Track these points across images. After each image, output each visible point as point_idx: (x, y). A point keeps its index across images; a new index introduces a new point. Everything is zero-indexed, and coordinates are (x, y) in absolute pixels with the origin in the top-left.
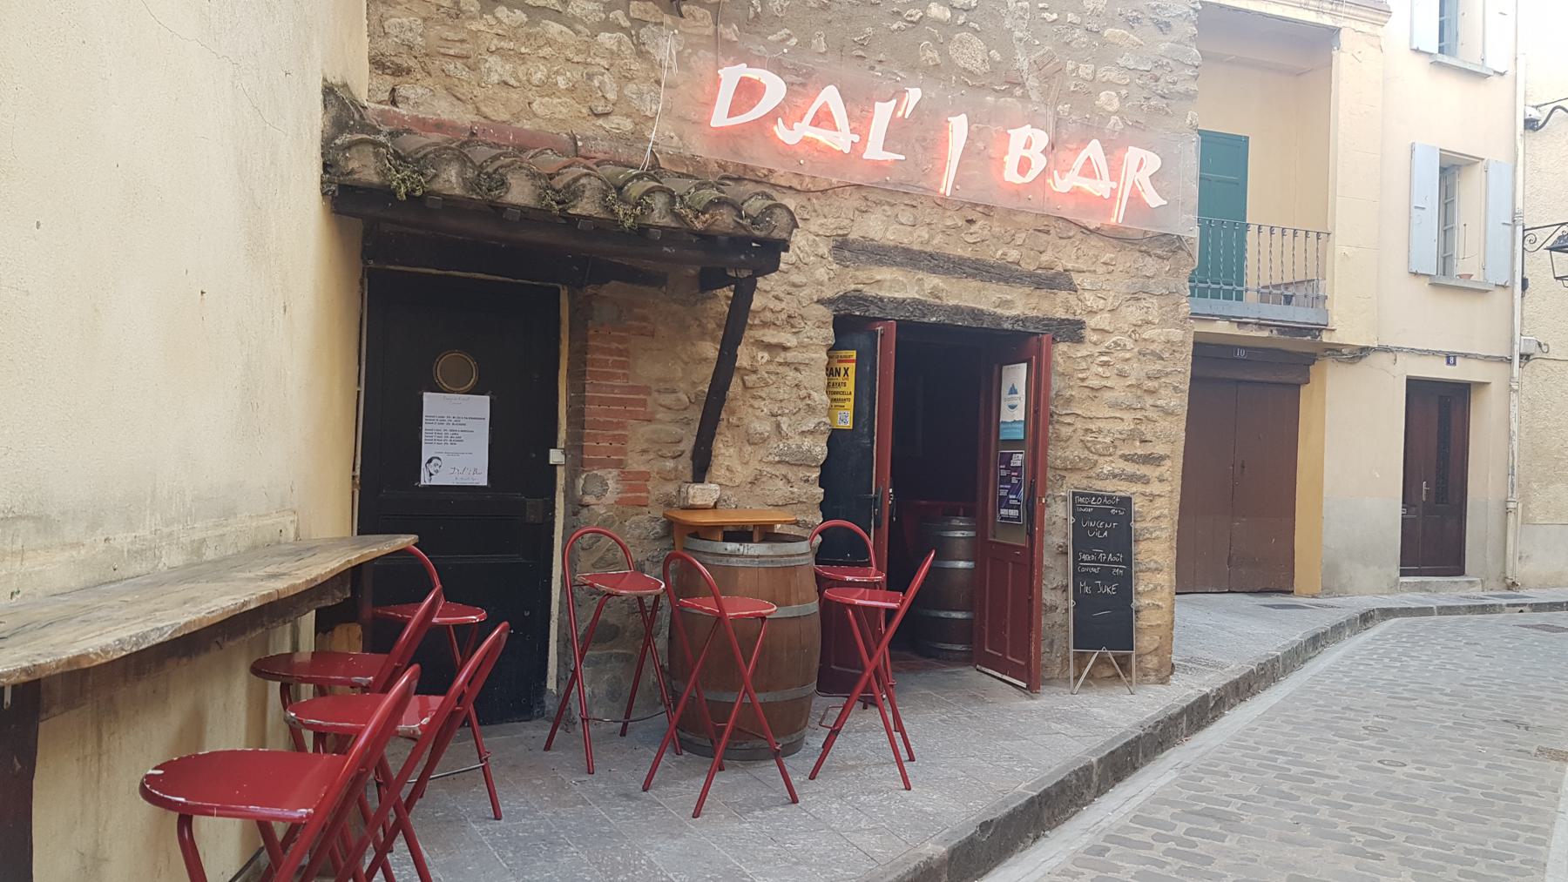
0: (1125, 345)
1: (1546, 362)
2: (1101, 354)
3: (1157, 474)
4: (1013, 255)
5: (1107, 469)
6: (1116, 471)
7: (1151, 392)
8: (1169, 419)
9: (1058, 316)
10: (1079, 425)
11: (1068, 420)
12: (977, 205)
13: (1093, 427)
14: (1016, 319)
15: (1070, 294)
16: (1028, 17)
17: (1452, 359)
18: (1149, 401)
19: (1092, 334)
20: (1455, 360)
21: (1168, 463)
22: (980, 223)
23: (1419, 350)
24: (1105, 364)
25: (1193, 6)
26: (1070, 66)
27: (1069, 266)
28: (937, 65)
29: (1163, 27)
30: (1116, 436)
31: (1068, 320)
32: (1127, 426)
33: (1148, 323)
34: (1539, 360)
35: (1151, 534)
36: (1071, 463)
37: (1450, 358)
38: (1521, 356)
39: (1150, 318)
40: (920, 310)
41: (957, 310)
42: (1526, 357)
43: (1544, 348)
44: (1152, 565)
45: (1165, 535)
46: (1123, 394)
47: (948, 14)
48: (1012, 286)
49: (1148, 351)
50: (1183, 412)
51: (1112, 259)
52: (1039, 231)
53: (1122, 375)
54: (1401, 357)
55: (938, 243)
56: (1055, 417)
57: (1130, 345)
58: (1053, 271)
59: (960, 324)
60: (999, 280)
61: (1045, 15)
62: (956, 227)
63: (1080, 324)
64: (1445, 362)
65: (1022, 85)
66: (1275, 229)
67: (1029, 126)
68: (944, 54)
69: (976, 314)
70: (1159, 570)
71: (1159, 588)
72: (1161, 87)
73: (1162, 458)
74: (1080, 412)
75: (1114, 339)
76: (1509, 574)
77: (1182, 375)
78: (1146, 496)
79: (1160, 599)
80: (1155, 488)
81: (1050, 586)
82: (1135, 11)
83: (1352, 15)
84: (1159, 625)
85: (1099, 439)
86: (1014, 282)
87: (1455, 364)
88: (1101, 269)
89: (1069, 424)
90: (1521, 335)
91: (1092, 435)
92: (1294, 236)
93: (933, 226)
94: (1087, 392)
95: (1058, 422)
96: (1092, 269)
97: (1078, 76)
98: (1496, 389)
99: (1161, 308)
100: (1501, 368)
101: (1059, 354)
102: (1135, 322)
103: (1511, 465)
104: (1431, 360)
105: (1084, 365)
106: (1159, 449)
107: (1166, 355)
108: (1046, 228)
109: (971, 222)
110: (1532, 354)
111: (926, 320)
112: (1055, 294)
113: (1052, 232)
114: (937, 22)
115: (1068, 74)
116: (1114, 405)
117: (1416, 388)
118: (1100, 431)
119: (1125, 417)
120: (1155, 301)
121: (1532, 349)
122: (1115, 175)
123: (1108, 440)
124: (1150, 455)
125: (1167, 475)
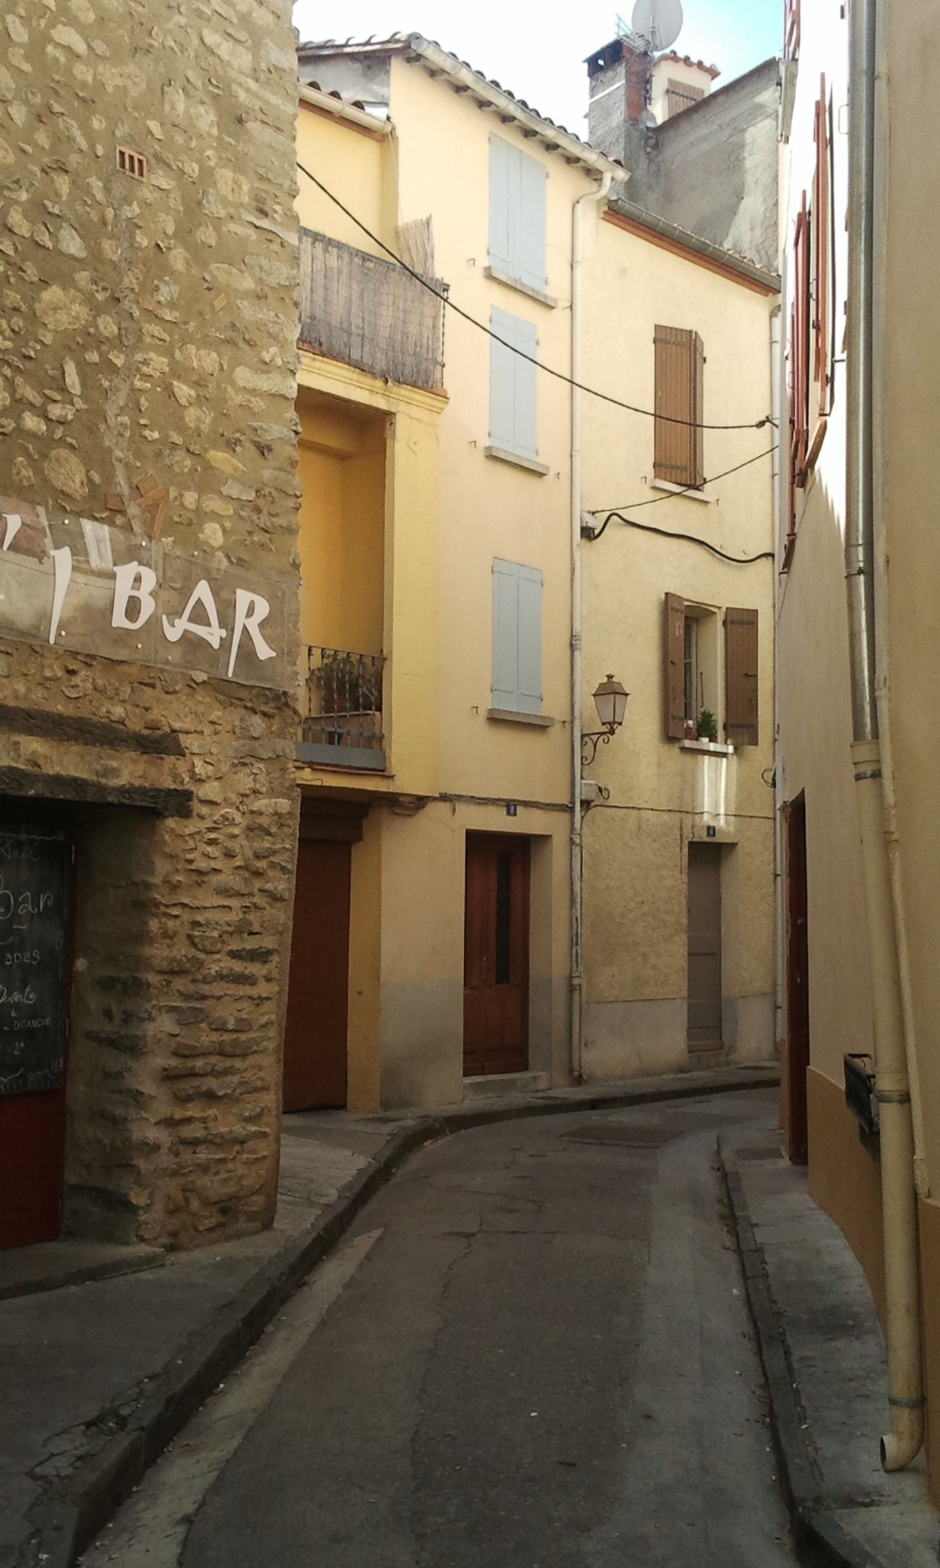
0: (233, 819)
1: (606, 809)
2: (210, 830)
3: (264, 972)
4: (118, 711)
5: (214, 969)
6: (224, 972)
7: (257, 874)
8: (278, 905)
9: (166, 785)
10: (187, 916)
11: (175, 911)
12: (77, 653)
13: (200, 918)
14: (122, 790)
15: (178, 759)
16: (128, 434)
17: (512, 808)
18: (258, 884)
19: (199, 805)
20: (515, 810)
21: (275, 958)
22: (83, 673)
23: (479, 799)
24: (212, 842)
25: (294, 428)
26: (173, 494)
27: (177, 725)
28: (32, 486)
29: (263, 450)
30: (224, 929)
31: (176, 790)
32: (234, 917)
33: (255, 792)
34: (599, 808)
35: (258, 1045)
36: (178, 964)
37: (511, 806)
38: (582, 802)
39: (258, 786)
40: (17, 780)
41: (58, 780)
42: (586, 804)
43: (605, 794)
44: (259, 1084)
45: (271, 1045)
46: (232, 877)
47: (44, 428)
48: (118, 751)
49: (257, 825)
50: (290, 896)
51: (219, 718)
52: (145, 684)
53: (229, 855)
54: (460, 807)
55: (38, 699)
56: (162, 908)
57: (238, 819)
58: (160, 732)
59: (61, 797)
60: (102, 744)
61: (147, 433)
62: (55, 679)
63: (188, 795)
64: (505, 813)
65: (122, 512)
66: (313, 649)
67: (136, 563)
68: (39, 471)
69: (78, 784)
70: (265, 1089)
71: (266, 1111)
72: (264, 520)
73: (269, 952)
74: (186, 901)
75: (222, 812)
76: (576, 1065)
77: (288, 853)
78: (254, 999)
79: (268, 1125)
80: (263, 989)
81: (153, 1121)
82: (238, 431)
83: (324, 371)
84: (265, 1157)
85: (206, 934)
86: (120, 745)
87: (515, 814)
88: (208, 730)
89: (176, 917)
90: (582, 778)
91: (200, 929)
92: (309, 655)
93: (30, 678)
94: (194, 877)
95: (165, 914)
96: (199, 729)
97: (182, 505)
98: (559, 843)
99: (269, 773)
100: (563, 818)
101: (167, 832)
102: (243, 792)
103: (575, 932)
104: (491, 809)
105: (192, 844)
106: (268, 942)
107: (273, 830)
108: (150, 681)
109: (72, 672)
110: (593, 801)
111: (22, 793)
112: (162, 759)
113: (158, 685)
114: (33, 435)
115: (171, 502)
116: (225, 892)
117: (477, 841)
118: (208, 924)
119: (232, 905)
120: (262, 766)
121: (592, 795)
122: (227, 622)
123: (215, 934)
124: (258, 949)
125: (275, 973)
